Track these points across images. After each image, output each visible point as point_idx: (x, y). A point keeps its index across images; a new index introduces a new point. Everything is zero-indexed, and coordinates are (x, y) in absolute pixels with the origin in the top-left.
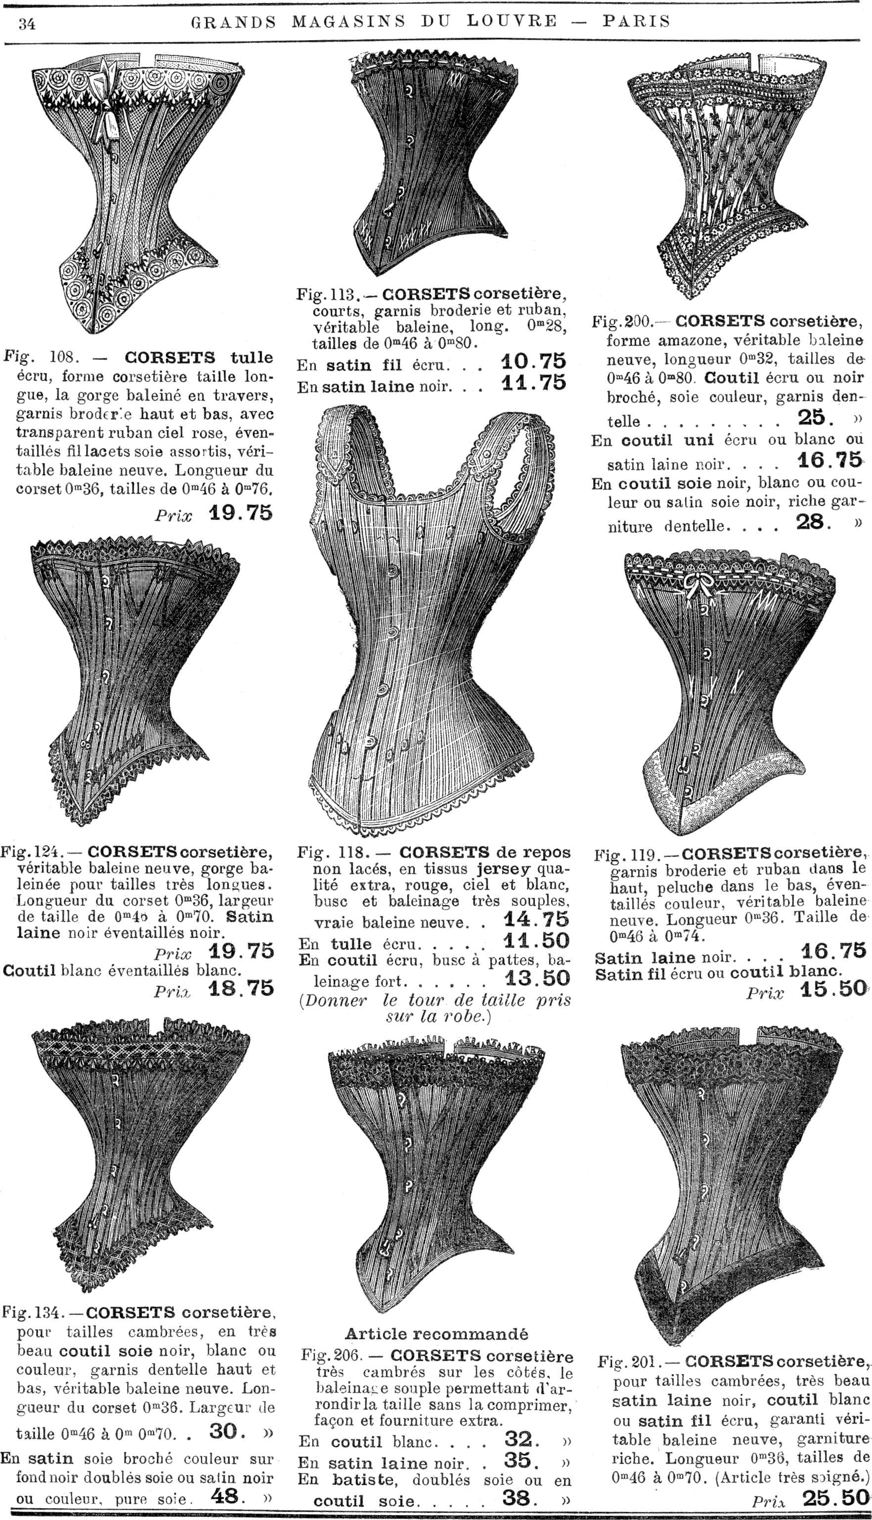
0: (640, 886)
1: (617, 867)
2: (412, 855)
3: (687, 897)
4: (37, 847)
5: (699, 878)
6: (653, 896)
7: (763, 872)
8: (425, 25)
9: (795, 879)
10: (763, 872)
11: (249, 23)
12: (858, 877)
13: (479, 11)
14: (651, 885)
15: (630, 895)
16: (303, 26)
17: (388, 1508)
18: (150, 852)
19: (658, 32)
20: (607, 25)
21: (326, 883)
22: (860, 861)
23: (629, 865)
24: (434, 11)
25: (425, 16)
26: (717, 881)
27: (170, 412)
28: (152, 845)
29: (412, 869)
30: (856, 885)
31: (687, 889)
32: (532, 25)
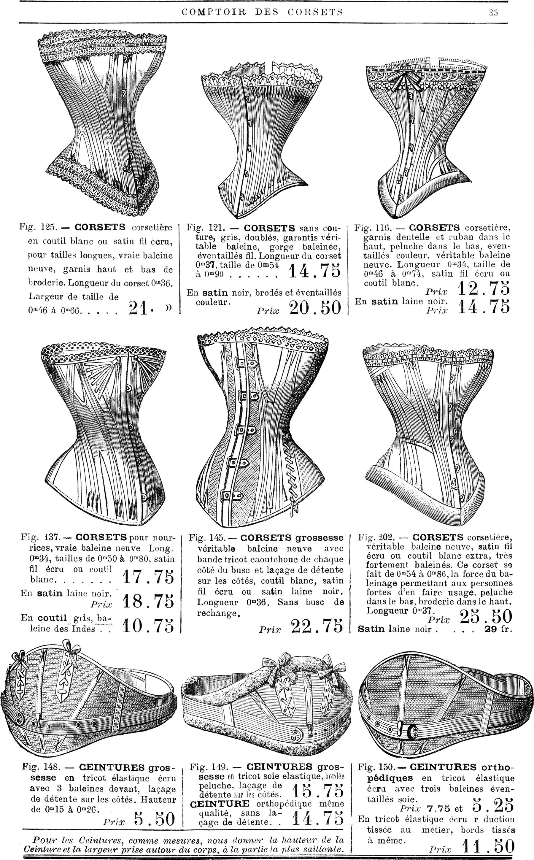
0: (381, 245)
1: (367, 235)
3: (408, 251)
4: (211, 225)
5: (415, 241)
6: (388, 251)
7: (452, 238)
9: (470, 242)
10: (452, 238)
12: (506, 242)
14: (386, 244)
15: (374, 250)
17: (333, 853)
21: (222, 812)
22: (507, 233)
23: (374, 233)
26: (425, 243)
27: (114, 268)
30: (505, 246)
31: (406, 247)
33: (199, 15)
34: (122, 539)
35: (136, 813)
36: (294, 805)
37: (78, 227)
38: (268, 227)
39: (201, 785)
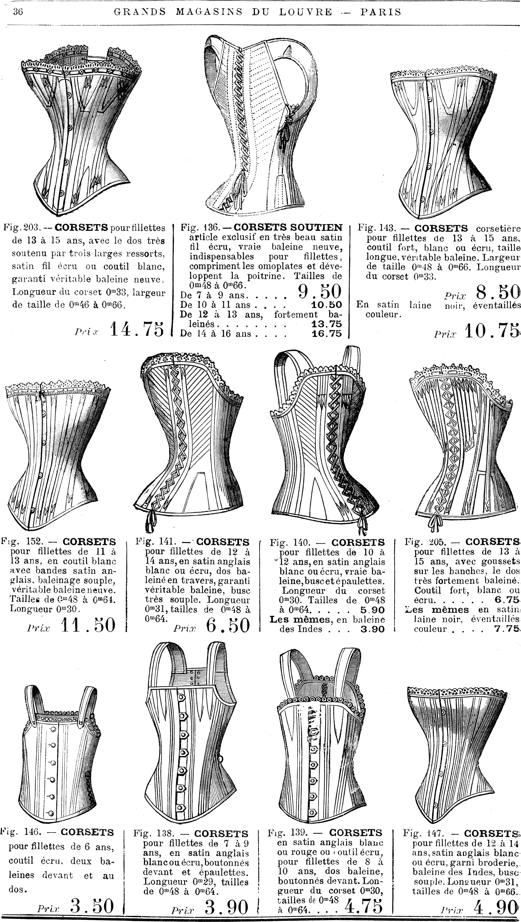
2: (472, 835)
8: (254, 14)
11: (149, 11)
13: (286, 6)
16: (182, 14)
18: (233, 542)
19: (394, 19)
20: (363, 15)
24: (259, 5)
25: (254, 9)
28: (101, 538)
29: (175, 580)
32: (317, 15)
33: (177, 14)
34: (102, 230)
35: (501, 286)
36: (204, 258)
37: (59, 227)
38: (221, 540)
39: (249, 275)
